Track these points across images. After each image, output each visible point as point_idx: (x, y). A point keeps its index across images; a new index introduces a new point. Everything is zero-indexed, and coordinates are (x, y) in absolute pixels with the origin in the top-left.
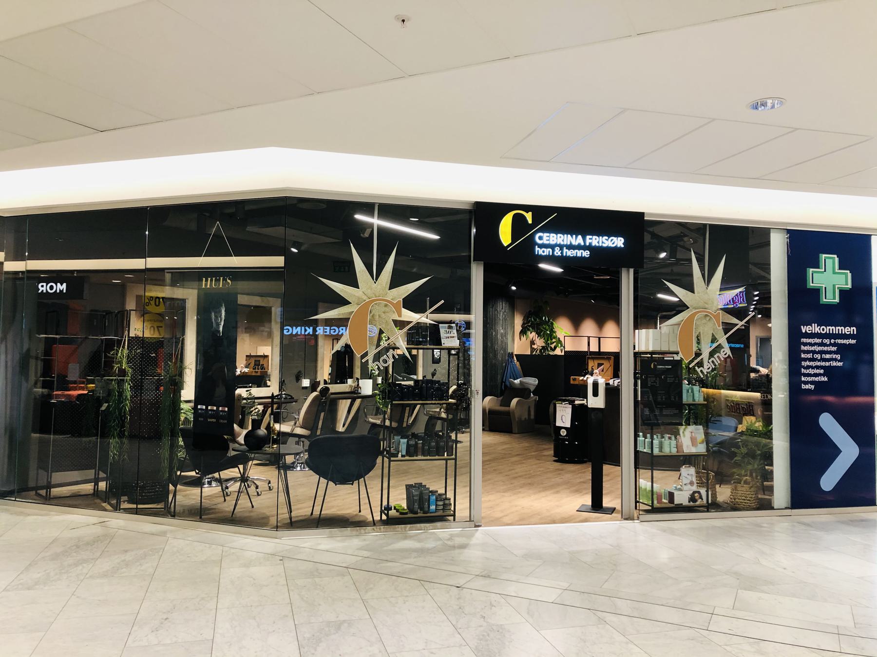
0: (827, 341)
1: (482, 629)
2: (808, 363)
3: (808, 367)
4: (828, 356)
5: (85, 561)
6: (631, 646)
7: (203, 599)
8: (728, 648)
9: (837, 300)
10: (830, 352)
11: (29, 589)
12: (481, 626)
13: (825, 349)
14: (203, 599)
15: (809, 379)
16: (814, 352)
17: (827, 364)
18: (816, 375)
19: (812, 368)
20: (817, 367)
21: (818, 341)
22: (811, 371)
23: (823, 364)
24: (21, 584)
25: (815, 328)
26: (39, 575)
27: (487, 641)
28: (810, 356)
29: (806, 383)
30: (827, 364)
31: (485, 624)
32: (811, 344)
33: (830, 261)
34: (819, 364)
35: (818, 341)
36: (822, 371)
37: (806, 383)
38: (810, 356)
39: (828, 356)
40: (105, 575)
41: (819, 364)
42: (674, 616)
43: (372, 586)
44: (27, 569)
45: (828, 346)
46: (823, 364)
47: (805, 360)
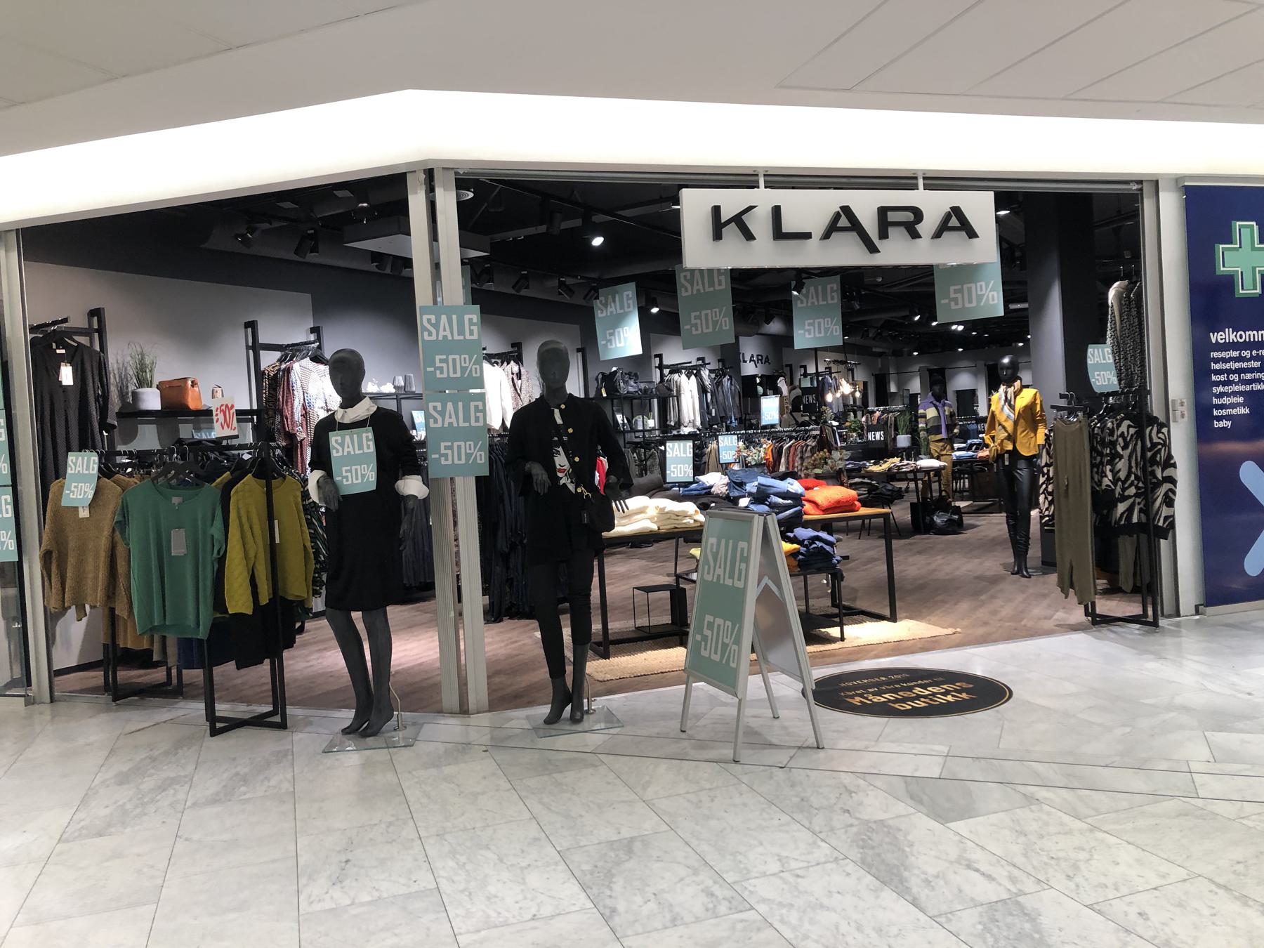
0: (1246, 354)
1: (854, 830)
2: (1221, 389)
3: (1221, 395)
4: (1249, 376)
5: (173, 781)
6: (1100, 835)
7: (391, 824)
8: (1245, 822)
9: (1259, 291)
10: (1251, 370)
11: (100, 835)
12: (851, 825)
13: (1245, 365)
14: (391, 824)
15: (1224, 412)
16: (1229, 372)
17: (1248, 388)
18: (1233, 406)
19: (1228, 395)
20: (1234, 394)
21: (1235, 354)
22: (1226, 400)
23: (1243, 388)
24: (83, 827)
25: (1229, 335)
26: (108, 811)
27: (873, 848)
28: (1223, 378)
29: (1219, 418)
30: (1248, 388)
31: (855, 822)
32: (1225, 360)
33: (1246, 229)
34: (1236, 388)
35: (1235, 354)
36: (1241, 400)
37: (1219, 418)
38: (1223, 378)
39: (1249, 376)
40: (214, 801)
41: (1236, 388)
42: (1138, 782)
43: (647, 778)
44: (84, 801)
45: (1249, 360)
46: (1243, 388)
47: (1217, 384)
